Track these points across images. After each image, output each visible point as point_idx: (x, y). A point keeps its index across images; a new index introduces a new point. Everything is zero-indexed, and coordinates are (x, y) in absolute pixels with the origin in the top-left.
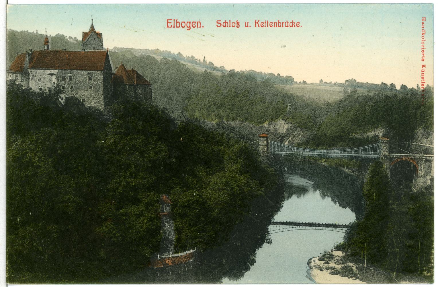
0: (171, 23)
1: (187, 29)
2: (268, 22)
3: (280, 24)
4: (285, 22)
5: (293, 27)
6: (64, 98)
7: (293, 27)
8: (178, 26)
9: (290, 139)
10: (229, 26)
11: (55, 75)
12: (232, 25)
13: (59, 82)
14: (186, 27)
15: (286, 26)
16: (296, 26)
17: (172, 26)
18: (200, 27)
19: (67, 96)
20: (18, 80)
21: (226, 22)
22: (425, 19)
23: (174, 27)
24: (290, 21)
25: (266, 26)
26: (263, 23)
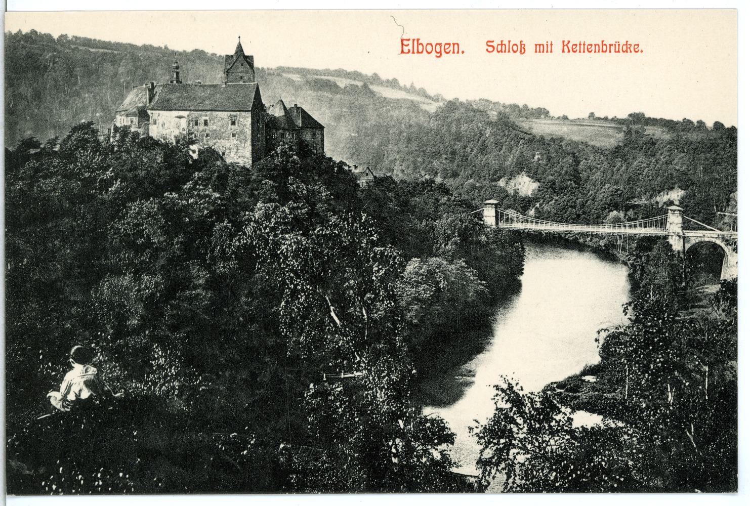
0: (408, 45)
1: (436, 56)
2: (584, 45)
3: (605, 47)
4: (614, 43)
5: (627, 52)
6: (197, 150)
7: (627, 52)
8: (604, 50)
9: (538, 205)
10: (507, 50)
11: (184, 117)
12: (513, 50)
13: (190, 128)
14: (434, 53)
15: (615, 52)
16: (632, 50)
17: (409, 51)
18: (458, 52)
19: (202, 148)
20: (133, 126)
21: (502, 45)
22: (566, 43)
23: (413, 52)
24: (622, 42)
25: (582, 50)
26: (576, 45)
